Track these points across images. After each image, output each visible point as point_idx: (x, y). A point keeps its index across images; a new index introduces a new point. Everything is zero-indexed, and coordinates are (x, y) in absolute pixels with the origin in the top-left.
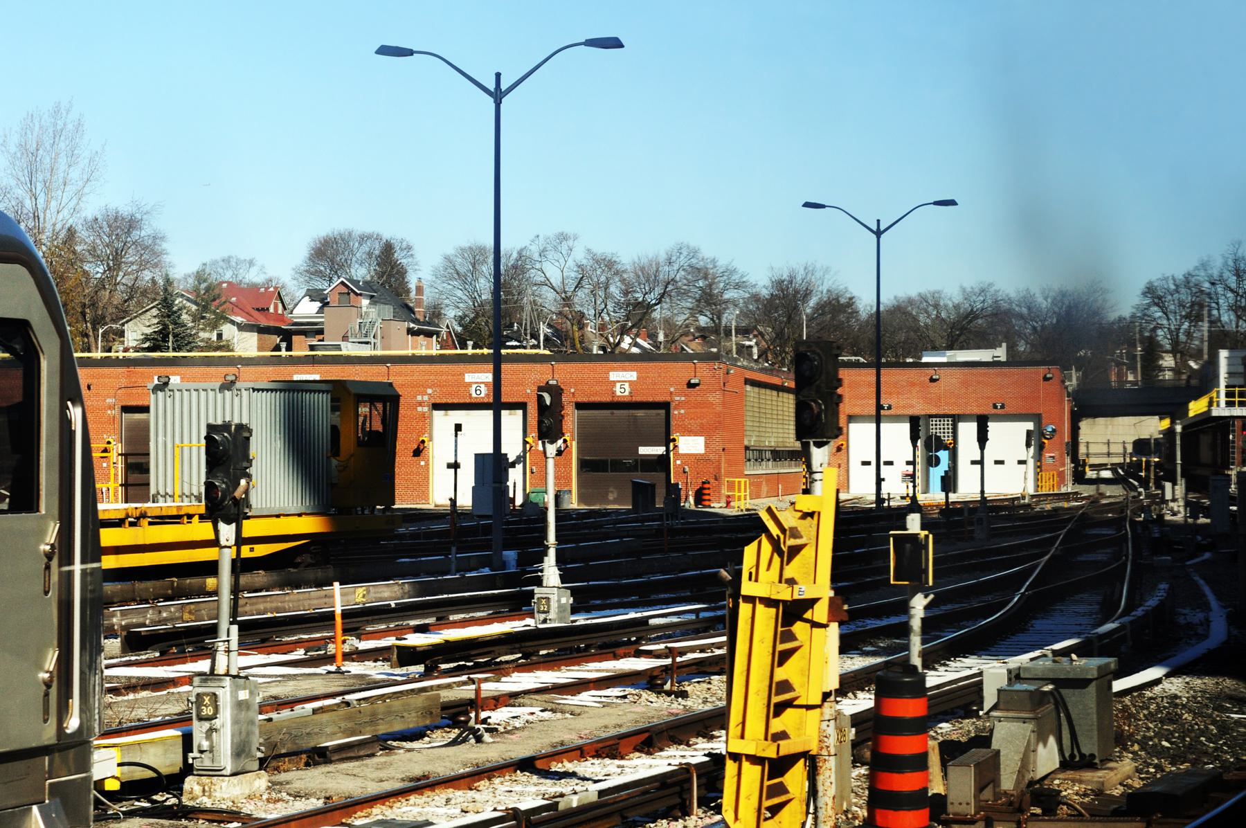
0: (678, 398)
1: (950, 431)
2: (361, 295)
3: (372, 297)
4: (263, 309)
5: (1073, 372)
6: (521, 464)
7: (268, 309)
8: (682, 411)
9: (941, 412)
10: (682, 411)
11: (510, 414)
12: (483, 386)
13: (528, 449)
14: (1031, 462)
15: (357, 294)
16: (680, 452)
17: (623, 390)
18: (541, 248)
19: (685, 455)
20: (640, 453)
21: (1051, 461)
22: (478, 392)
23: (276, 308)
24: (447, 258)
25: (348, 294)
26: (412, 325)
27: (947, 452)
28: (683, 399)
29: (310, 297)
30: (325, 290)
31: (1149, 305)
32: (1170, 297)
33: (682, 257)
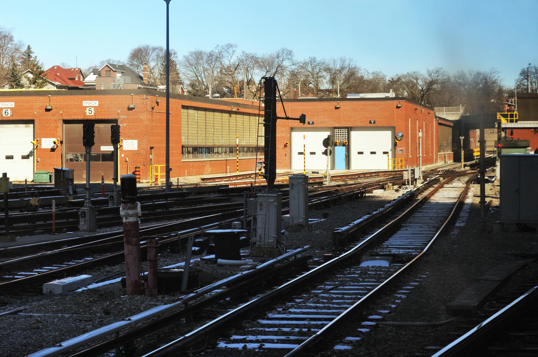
0: (122, 117)
1: (346, 138)
2: (116, 71)
3: (123, 72)
4: (72, 79)
5: (461, 107)
6: (33, 157)
7: (74, 79)
8: (125, 125)
9: (341, 126)
10: (125, 125)
11: (26, 127)
12: (9, 110)
13: (35, 148)
14: (390, 153)
15: (114, 71)
16: (124, 149)
17: (90, 112)
18: (220, 51)
19: (127, 151)
20: (101, 150)
21: (401, 152)
22: (7, 114)
23: (79, 78)
24: (185, 57)
25: (110, 71)
26: (140, 86)
27: (344, 147)
28: (125, 117)
29: (94, 72)
30: (99, 69)
31: (523, 80)
32: (532, 76)
33: (284, 55)
